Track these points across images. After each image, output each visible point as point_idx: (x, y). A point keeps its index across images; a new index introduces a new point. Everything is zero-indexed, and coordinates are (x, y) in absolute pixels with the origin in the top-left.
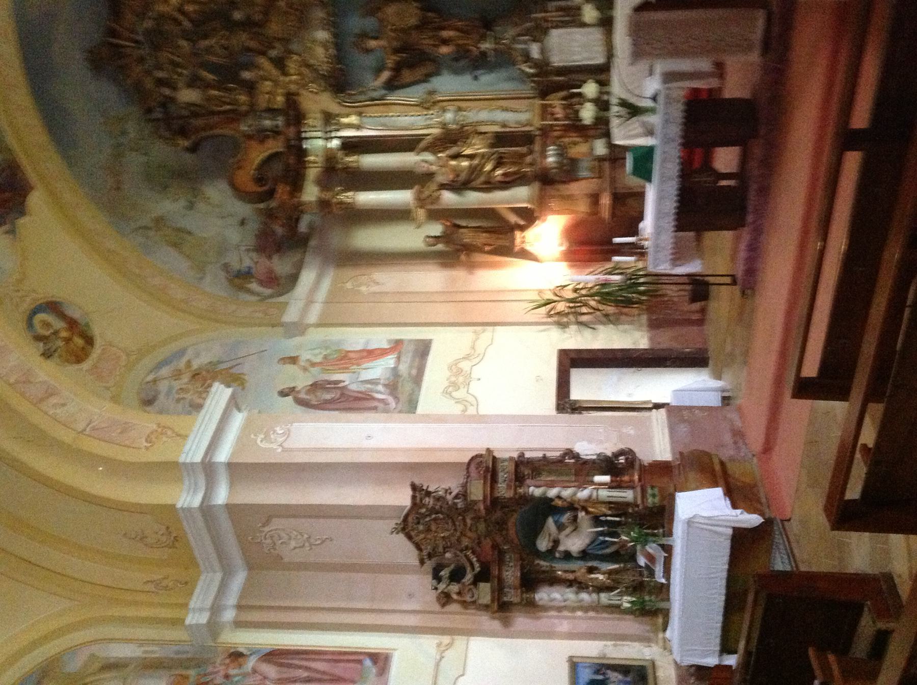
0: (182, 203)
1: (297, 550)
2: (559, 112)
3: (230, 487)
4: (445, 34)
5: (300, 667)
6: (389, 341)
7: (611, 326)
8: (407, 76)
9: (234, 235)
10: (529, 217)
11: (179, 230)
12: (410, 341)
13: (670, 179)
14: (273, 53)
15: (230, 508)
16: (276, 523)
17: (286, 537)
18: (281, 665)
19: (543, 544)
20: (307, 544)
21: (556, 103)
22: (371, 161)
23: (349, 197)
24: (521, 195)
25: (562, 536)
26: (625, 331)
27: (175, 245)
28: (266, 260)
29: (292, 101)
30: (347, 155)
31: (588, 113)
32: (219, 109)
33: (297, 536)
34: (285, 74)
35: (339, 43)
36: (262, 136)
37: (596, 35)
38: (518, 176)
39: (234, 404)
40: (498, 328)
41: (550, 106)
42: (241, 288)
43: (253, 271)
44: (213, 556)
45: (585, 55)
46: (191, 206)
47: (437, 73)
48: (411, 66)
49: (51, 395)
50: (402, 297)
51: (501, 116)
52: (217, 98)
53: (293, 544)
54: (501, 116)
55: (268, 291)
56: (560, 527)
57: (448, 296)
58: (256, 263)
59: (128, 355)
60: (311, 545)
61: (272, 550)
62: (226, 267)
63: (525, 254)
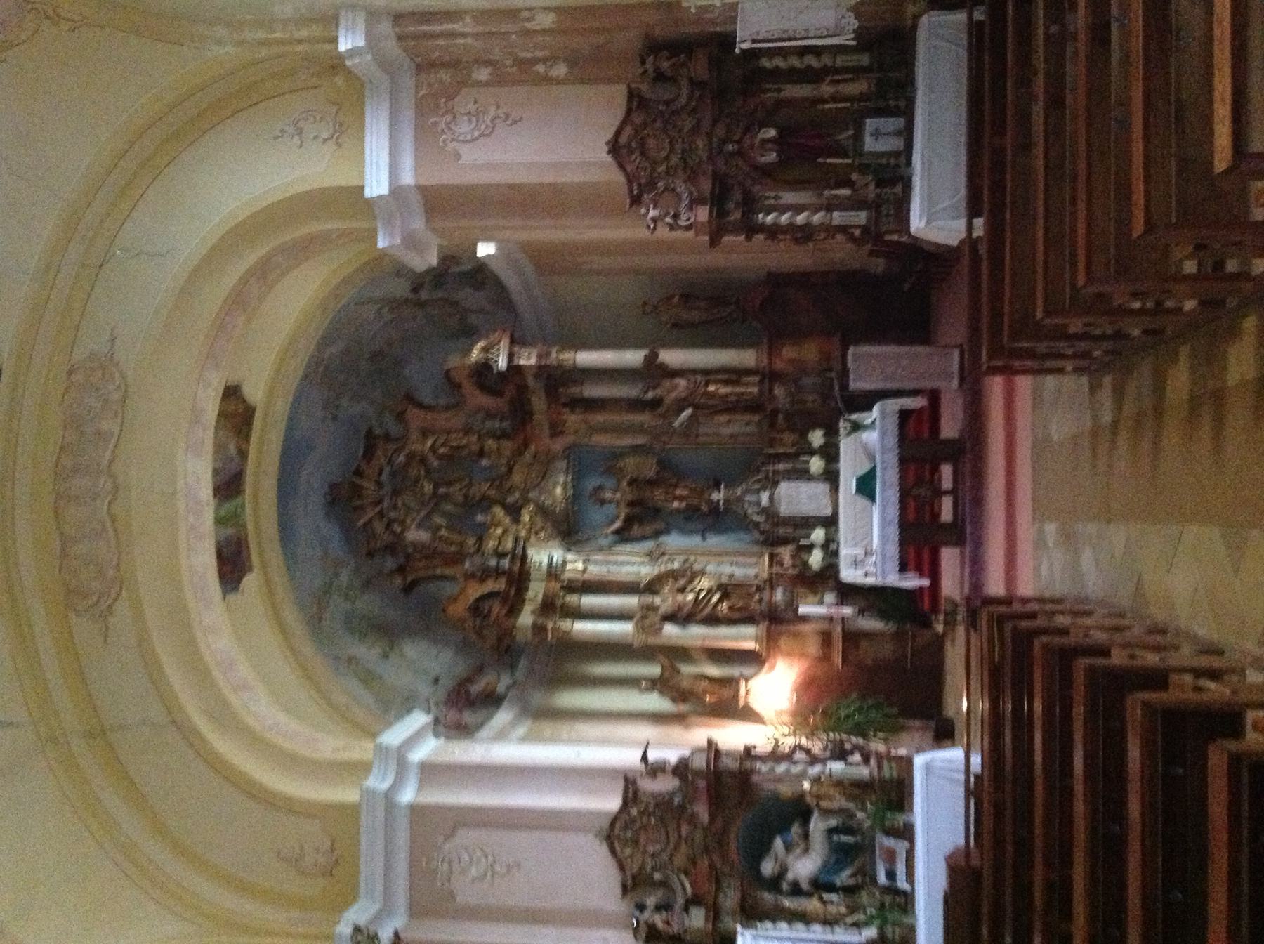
2: (787, 561)
3: (418, 790)
4: (678, 492)
8: (636, 530)
10: (754, 659)
14: (510, 500)
15: (416, 811)
16: (466, 837)
17: (467, 858)
19: (768, 868)
20: (489, 874)
21: (786, 553)
22: (590, 601)
23: (566, 624)
24: (745, 638)
25: (790, 859)
35: (575, 498)
36: (485, 574)
37: (822, 488)
44: (380, 888)
46: (386, 656)
47: (667, 531)
51: (727, 569)
53: (474, 871)
56: (789, 847)
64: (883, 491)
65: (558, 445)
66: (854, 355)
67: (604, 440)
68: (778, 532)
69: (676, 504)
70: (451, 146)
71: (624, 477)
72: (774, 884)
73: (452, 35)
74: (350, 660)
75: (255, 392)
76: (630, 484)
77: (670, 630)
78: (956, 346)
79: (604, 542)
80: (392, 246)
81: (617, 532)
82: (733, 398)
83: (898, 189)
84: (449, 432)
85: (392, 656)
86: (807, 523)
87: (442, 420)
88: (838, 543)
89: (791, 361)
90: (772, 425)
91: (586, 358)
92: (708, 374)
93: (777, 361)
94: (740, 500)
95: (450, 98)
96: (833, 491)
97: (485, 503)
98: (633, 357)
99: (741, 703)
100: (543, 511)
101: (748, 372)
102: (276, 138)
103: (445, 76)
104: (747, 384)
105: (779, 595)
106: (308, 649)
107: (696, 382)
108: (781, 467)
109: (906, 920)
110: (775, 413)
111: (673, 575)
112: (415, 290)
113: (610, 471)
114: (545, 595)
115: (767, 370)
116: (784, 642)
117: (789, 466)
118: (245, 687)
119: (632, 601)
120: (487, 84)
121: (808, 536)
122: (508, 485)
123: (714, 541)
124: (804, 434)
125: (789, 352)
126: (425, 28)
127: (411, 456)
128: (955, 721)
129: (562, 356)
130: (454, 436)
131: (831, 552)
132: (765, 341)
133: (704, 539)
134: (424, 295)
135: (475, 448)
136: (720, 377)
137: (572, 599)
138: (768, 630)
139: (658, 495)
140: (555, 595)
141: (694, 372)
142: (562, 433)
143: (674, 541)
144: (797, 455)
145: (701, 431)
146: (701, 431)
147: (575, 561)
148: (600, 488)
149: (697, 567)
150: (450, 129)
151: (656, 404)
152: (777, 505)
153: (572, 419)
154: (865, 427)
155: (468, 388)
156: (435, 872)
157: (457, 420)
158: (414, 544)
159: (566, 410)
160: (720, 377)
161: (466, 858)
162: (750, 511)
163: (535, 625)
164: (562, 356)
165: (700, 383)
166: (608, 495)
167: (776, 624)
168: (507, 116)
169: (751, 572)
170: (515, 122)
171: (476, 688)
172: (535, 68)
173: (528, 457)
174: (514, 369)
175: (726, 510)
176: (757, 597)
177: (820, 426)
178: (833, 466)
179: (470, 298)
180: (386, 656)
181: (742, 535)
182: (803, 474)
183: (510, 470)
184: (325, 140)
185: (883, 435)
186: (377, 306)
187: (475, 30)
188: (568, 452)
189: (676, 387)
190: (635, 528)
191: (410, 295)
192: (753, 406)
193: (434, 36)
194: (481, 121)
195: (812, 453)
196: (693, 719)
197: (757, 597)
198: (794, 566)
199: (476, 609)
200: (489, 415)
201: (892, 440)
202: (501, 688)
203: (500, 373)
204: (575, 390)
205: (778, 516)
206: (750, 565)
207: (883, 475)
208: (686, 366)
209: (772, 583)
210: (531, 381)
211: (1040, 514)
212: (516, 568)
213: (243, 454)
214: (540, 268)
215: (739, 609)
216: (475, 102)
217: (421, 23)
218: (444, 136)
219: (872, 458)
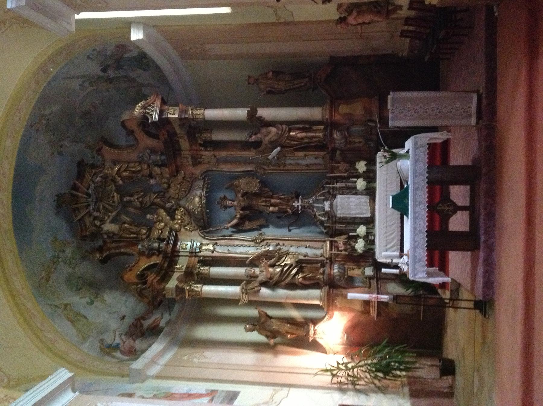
0: (87, 299)
2: (342, 246)
6: (207, 390)
7: (381, 395)
8: (247, 225)
9: (114, 324)
11: (78, 314)
12: (223, 391)
14: (168, 205)
21: (340, 241)
22: (215, 271)
23: (198, 287)
26: (392, 399)
27: (72, 322)
28: (132, 341)
30: (203, 266)
31: (360, 246)
32: (128, 236)
34: (173, 218)
35: (209, 203)
36: (151, 253)
37: (365, 199)
38: (312, 282)
39: (71, 384)
40: (292, 390)
41: (336, 241)
42: (108, 354)
43: (120, 346)
45: (358, 211)
47: (267, 226)
50: (221, 366)
51: (303, 250)
54: (303, 250)
55: (126, 358)
57: (257, 368)
58: (124, 343)
59: (9, 381)
62: (102, 341)
63: (315, 346)
64: (415, 206)
65: (198, 171)
66: (393, 98)
67: (226, 168)
68: (335, 227)
69: (271, 209)
71: (239, 191)
76: (243, 196)
77: (265, 291)
78: (474, 92)
79: (227, 232)
80: (18, 7)
81: (234, 226)
82: (306, 140)
84: (128, 163)
85: (96, 303)
86: (356, 222)
87: (125, 155)
88: (375, 236)
89: (345, 114)
90: (332, 159)
91: (211, 114)
92: (291, 124)
93: (336, 115)
94: (311, 207)
96: (372, 201)
97: (153, 207)
98: (241, 113)
99: (311, 339)
100: (188, 212)
101: (319, 123)
104: (315, 131)
105: (336, 270)
106: (30, 304)
107: (283, 129)
108: (338, 185)
110: (334, 150)
111: (267, 255)
112: (104, 70)
113: (232, 188)
114: (187, 267)
115: (329, 121)
116: (338, 301)
117: (343, 185)
119: (240, 271)
121: (355, 231)
122: (167, 195)
123: (296, 232)
124: (352, 164)
125: (343, 109)
127: (105, 177)
128: (457, 363)
129: (195, 112)
130: (133, 165)
131: (370, 241)
132: (328, 101)
133: (290, 230)
134: (111, 73)
135: (147, 172)
136: (298, 126)
137: (204, 269)
138: (328, 294)
139: (261, 203)
140: (194, 267)
141: (282, 123)
142: (200, 163)
143: (270, 232)
144: (348, 178)
145: (288, 162)
146: (288, 162)
147: (208, 244)
148: (225, 198)
149: (284, 249)
151: (257, 145)
152: (335, 210)
153: (206, 154)
154: (401, 156)
155: (139, 134)
157: (134, 156)
158: (108, 233)
159: (203, 148)
160: (298, 126)
162: (317, 214)
163: (177, 287)
164: (195, 112)
165: (285, 130)
166: (229, 203)
167: (334, 288)
169: (319, 252)
171: (146, 323)
173: (180, 178)
174: (164, 122)
175: (303, 212)
176: (321, 271)
177: (364, 160)
178: (372, 185)
179: (138, 74)
180: (92, 302)
181: (313, 228)
182: (353, 191)
183: (169, 187)
188: (205, 175)
189: (270, 132)
190: (247, 223)
191: (102, 74)
192: (320, 146)
195: (358, 177)
196: (280, 348)
197: (321, 271)
198: (345, 250)
199: (142, 277)
200: (153, 151)
201: (423, 166)
202: (162, 323)
203: (154, 123)
204: (206, 136)
205: (336, 216)
206: (318, 248)
207: (415, 195)
208: (277, 119)
209: (331, 260)
212: (170, 248)
214: (184, 55)
215: (310, 279)
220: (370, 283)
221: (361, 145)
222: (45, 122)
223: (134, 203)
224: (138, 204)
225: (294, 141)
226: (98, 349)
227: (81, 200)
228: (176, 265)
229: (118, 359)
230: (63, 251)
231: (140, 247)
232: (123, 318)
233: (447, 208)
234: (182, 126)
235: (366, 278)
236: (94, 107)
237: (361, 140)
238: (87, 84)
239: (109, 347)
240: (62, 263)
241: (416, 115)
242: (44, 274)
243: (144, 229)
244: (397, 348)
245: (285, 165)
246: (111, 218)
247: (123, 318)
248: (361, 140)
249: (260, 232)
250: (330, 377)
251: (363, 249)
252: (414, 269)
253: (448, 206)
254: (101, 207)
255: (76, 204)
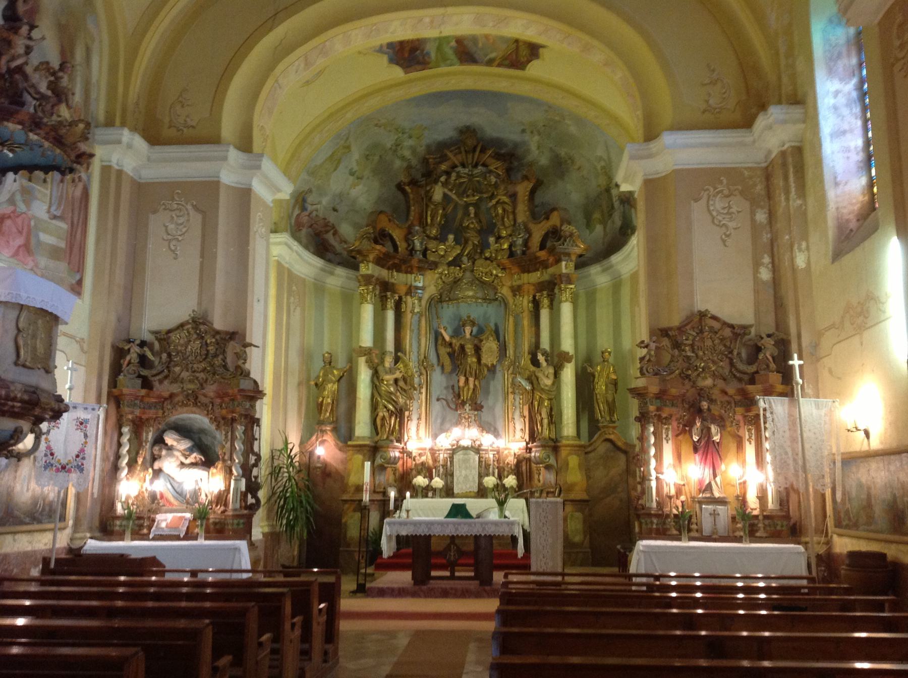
1: (164, 229)
5: (79, 219)
8: (443, 351)
11: (339, 162)
13: (457, 529)
16: (196, 219)
17: (180, 222)
18: (81, 199)
20: (170, 237)
22: (390, 315)
29: (434, 266)
33: (181, 231)
34: (450, 264)
48: (451, 355)
49: (306, 64)
52: (437, 213)
53: (171, 227)
55: (293, 221)
60: (170, 241)
61: (164, 207)
64: (454, 524)
70: (705, 195)
72: (159, 441)
73: (787, 192)
74: (348, 148)
75: (534, 69)
83: (675, 532)
88: (432, 498)
93: (567, 452)
95: (742, 193)
102: (708, 66)
103: (760, 188)
109: (128, 534)
114: (393, 284)
118: (308, 64)
119: (390, 346)
120: (753, 220)
125: (574, 461)
126: (791, 170)
137: (390, 304)
142: (515, 295)
147: (420, 306)
150: (718, 193)
151: (535, 362)
153: (525, 302)
156: (173, 199)
159: (531, 298)
161: (181, 220)
168: (728, 236)
170: (724, 241)
172: (766, 256)
184: (707, 101)
185: (495, 524)
186: (606, 158)
187: (791, 208)
193: (786, 178)
194: (724, 216)
204: (545, 302)
207: (465, 524)
210: (551, 270)
211: (419, 635)
213: (490, 63)
216: (739, 212)
217: (795, 167)
218: (712, 189)
219: (478, 516)
220: (378, 493)
221: (536, 481)
222: (557, 118)
223: (466, 218)
224: (466, 224)
225: (539, 405)
226: (302, 190)
227: (470, 156)
228: (396, 271)
229: (292, 213)
230: (410, 137)
231: (417, 228)
232: (335, 210)
233: (452, 554)
234: (553, 276)
235: (384, 488)
236: (579, 169)
237: (542, 482)
238: (603, 164)
239: (304, 200)
240: (396, 137)
241: (541, 524)
242: (383, 121)
243: (437, 231)
244: (312, 519)
245: (514, 393)
246: (449, 193)
247: (335, 210)
248: (542, 482)
249: (436, 366)
250: (280, 448)
251: (417, 484)
252: (394, 523)
253: (454, 555)
254: (462, 180)
255: (466, 151)
